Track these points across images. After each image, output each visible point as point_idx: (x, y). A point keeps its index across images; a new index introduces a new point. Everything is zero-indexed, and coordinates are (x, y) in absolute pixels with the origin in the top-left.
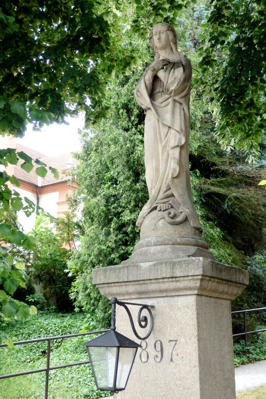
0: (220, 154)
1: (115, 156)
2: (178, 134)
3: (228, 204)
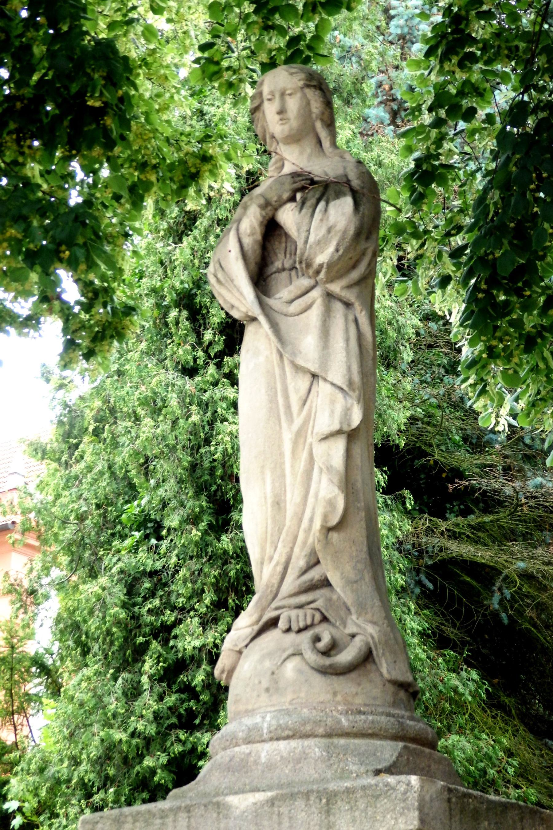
0: (474, 441)
1: (156, 451)
2: (340, 395)
3: (502, 594)
